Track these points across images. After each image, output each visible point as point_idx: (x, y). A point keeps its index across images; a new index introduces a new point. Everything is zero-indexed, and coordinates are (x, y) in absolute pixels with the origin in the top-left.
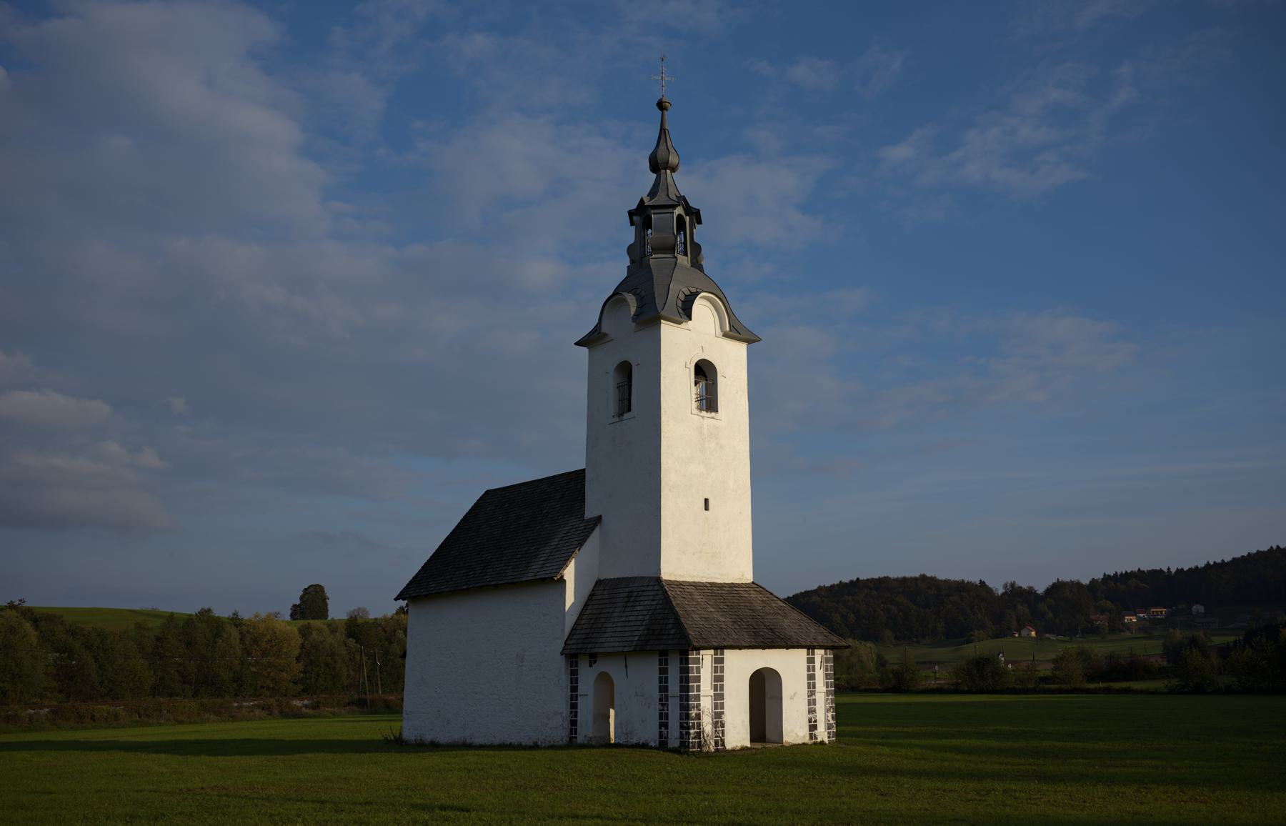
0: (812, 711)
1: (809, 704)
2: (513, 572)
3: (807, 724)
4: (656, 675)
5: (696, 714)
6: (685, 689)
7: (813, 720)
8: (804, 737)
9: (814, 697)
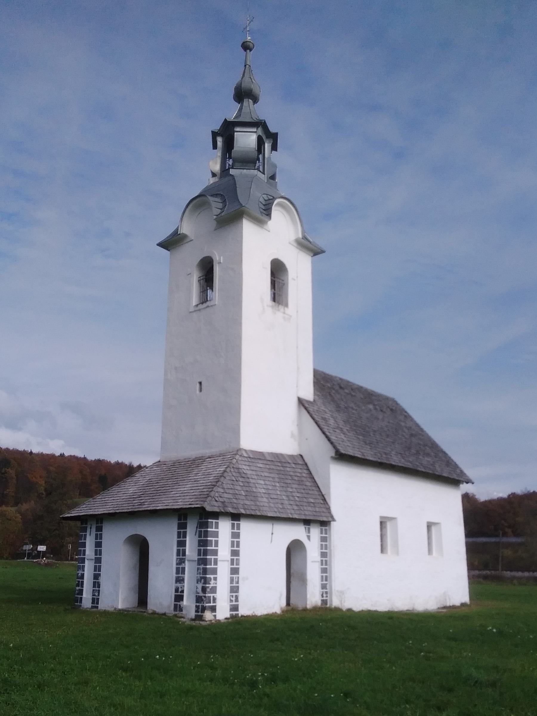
0: (180, 580)
1: (178, 572)
2: (223, 461)
3: (173, 594)
4: (175, 540)
5: (81, 574)
6: (203, 561)
7: (180, 590)
8: (207, 612)
9: (183, 565)
